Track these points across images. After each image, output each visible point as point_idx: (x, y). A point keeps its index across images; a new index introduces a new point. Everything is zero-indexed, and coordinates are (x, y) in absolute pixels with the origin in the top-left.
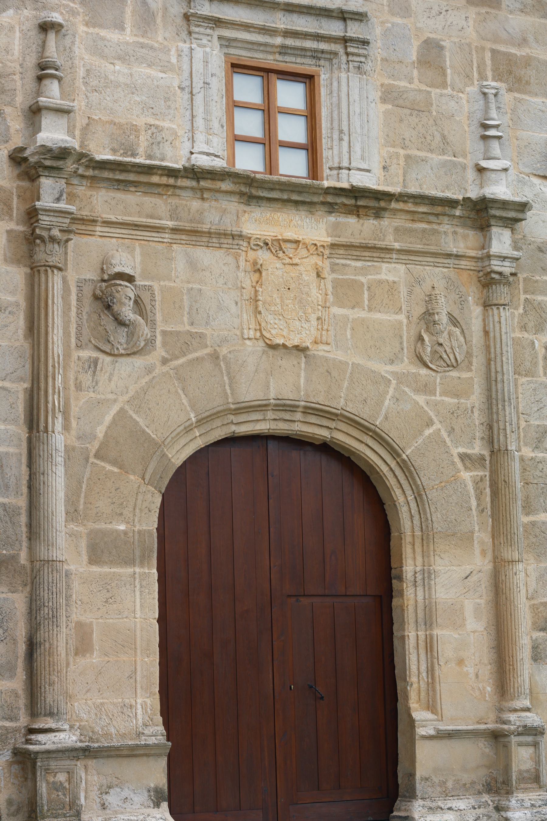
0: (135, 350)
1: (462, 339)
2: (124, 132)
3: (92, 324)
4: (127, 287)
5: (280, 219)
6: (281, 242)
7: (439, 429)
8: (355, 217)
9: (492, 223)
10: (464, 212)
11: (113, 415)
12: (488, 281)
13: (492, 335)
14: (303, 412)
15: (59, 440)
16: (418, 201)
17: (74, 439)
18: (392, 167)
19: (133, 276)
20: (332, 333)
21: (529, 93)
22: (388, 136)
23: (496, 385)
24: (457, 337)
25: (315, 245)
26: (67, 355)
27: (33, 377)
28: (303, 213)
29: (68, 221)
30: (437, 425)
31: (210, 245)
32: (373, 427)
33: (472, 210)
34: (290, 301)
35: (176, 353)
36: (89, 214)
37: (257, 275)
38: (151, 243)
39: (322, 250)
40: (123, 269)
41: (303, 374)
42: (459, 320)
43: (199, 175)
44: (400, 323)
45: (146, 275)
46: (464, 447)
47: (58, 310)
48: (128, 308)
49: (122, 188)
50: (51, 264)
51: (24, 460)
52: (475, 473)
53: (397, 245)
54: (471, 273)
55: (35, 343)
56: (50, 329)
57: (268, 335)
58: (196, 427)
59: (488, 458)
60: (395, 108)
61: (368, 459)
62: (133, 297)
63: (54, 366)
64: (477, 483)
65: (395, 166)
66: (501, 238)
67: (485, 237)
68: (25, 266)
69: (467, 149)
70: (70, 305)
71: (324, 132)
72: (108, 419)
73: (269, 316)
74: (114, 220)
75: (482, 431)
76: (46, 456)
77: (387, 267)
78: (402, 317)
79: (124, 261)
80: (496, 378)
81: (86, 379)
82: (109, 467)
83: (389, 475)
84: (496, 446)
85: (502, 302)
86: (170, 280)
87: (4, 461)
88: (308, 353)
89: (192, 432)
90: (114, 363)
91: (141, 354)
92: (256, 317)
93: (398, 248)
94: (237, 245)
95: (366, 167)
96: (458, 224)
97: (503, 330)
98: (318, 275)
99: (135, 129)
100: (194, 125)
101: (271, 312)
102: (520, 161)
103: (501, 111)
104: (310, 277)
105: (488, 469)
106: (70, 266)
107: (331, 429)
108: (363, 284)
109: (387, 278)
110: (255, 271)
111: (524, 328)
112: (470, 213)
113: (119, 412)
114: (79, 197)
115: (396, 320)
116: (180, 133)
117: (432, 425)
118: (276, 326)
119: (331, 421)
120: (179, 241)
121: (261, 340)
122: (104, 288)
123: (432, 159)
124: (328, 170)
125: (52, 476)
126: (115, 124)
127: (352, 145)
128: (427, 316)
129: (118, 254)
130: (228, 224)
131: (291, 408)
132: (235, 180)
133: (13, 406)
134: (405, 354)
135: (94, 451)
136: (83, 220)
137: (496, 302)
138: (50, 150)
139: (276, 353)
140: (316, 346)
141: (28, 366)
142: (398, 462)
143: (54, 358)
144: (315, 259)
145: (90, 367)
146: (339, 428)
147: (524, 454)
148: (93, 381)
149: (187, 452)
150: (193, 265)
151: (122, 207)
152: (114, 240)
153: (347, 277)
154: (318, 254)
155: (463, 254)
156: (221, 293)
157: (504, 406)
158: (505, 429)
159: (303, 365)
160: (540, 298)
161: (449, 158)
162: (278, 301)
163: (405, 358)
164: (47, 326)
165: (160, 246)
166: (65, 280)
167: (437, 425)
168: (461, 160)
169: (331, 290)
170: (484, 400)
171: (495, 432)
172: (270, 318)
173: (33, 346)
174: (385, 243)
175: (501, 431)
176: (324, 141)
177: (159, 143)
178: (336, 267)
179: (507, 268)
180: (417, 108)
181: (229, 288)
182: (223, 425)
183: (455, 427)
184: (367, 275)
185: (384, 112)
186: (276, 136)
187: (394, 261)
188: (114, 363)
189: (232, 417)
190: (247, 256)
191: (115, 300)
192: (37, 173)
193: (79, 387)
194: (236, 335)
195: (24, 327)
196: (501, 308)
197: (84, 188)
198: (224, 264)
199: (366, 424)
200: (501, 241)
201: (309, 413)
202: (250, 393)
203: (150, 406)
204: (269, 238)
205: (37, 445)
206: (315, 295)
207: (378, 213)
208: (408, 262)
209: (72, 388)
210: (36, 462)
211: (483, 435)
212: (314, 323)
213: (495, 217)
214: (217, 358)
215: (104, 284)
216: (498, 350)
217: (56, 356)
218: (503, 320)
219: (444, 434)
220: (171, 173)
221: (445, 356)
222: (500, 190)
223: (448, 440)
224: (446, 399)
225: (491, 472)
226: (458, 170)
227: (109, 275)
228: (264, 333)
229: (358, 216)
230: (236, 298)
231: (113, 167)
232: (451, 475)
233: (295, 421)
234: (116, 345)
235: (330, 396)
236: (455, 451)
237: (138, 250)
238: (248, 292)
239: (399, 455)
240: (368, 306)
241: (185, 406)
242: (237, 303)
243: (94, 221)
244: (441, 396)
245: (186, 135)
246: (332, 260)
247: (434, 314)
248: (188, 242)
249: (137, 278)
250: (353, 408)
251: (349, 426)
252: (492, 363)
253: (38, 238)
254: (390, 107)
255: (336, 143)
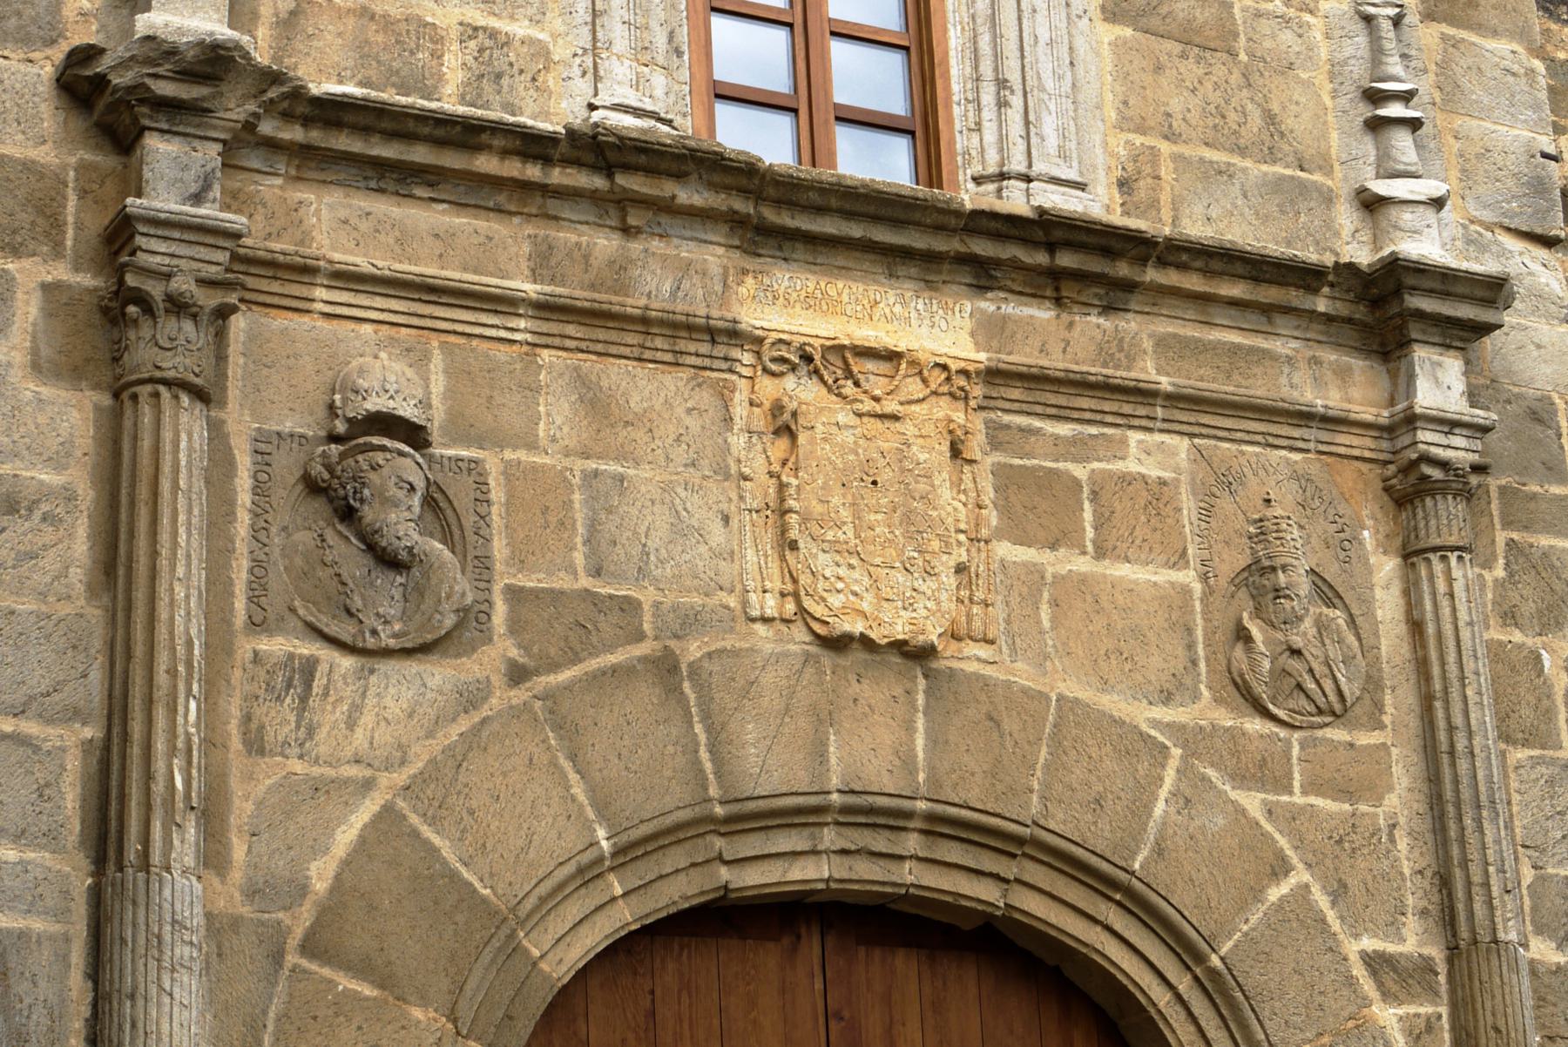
0: (429, 637)
1: (1351, 639)
2: (398, 42)
3: (298, 561)
4: (401, 454)
5: (845, 298)
6: (848, 355)
7: (1307, 886)
8: (1048, 304)
9: (1414, 335)
10: (1338, 304)
11: (359, 825)
12: (1411, 486)
13: (1431, 629)
14: (923, 832)
15: (183, 892)
16: (1216, 265)
17: (237, 894)
18: (1141, 183)
19: (422, 428)
20: (998, 612)
21: (1478, 28)
22: (1125, 103)
23: (1453, 764)
24: (1339, 632)
25: (945, 367)
26: (219, 644)
27: (110, 705)
28: (908, 285)
29: (222, 257)
30: (1300, 875)
31: (648, 355)
32: (1123, 876)
33: (1359, 299)
34: (880, 517)
35: (552, 651)
36: (291, 248)
37: (783, 443)
38: (475, 342)
39: (962, 382)
40: (391, 404)
41: (920, 723)
42: (1340, 590)
43: (612, 156)
44: (1185, 591)
45: (461, 431)
46: (1376, 936)
47: (190, 511)
48: (407, 515)
49: (391, 187)
50: (171, 374)
51: (78, 956)
52: (1412, 1009)
53: (1165, 383)
54: (1365, 467)
55: (120, 606)
56: (163, 563)
57: (818, 610)
58: (612, 869)
59: (1442, 968)
60: (1138, 35)
61: (1112, 970)
62: (420, 484)
63: (172, 672)
64: (1418, 1037)
65: (1149, 180)
66: (1439, 374)
67: (1393, 376)
68: (96, 387)
69: (1333, 152)
70: (231, 503)
71: (955, 87)
72: (345, 837)
73: (821, 556)
74: (366, 268)
75: (1420, 893)
76: (142, 941)
77: (1140, 442)
78: (1188, 577)
79: (392, 378)
80: (1452, 745)
81: (280, 719)
82: (345, 983)
83: (1175, 1016)
84: (1464, 933)
85: (1453, 540)
86: (532, 446)
87: (13, 960)
88: (934, 665)
89: (600, 883)
90: (362, 674)
91: (445, 654)
92: (783, 558)
93: (1170, 389)
94: (726, 359)
95: (1072, 175)
96: (1321, 338)
97: (1463, 616)
98: (956, 452)
99: (433, 36)
100: (600, 35)
101: (826, 546)
102: (1467, 192)
103: (1413, 64)
104: (931, 454)
105: (1445, 997)
106: (233, 392)
107: (1006, 881)
108: (1077, 483)
109: (1143, 470)
110: (777, 432)
111: (1510, 617)
112: (1353, 307)
113: (378, 819)
114: (264, 205)
115: (1172, 583)
116: (559, 52)
117: (1287, 873)
118: (840, 585)
119: (1004, 859)
120: (557, 342)
121: (800, 623)
122: (335, 459)
123: (1244, 170)
124: (971, 185)
125: (159, 1005)
126: (372, 18)
127: (1032, 118)
128: (1256, 578)
129: (378, 364)
130: (697, 303)
131: (891, 819)
132: (716, 178)
133: (47, 792)
134: (1203, 677)
135: (299, 933)
136: (272, 264)
137: (1438, 542)
138: (172, 52)
139: (845, 661)
140: (954, 645)
141: (96, 676)
142: (1196, 978)
143: (173, 649)
144: (943, 409)
145: (289, 685)
146: (1027, 878)
147: (1537, 957)
148: (298, 727)
149: (589, 942)
150: (596, 405)
151: (391, 241)
152: (367, 328)
153: (1035, 462)
154: (951, 394)
155: (1343, 414)
156: (680, 490)
157: (1479, 821)
158: (1486, 885)
159: (921, 699)
160: (1545, 541)
161: (1289, 172)
162: (845, 514)
163: (1202, 687)
164: (154, 554)
165: (502, 353)
166: (216, 430)
167: (1300, 875)
168: (1316, 177)
169: (992, 495)
170: (1422, 807)
171: (1460, 894)
172: (823, 562)
173: (114, 615)
174: (1133, 375)
175: (1475, 889)
176: (957, 111)
177: (499, 76)
178: (1002, 436)
179: (1459, 450)
180: (1197, 40)
181: (705, 477)
182: (693, 865)
183: (1349, 881)
184: (1087, 460)
185: (1115, 44)
186: (828, 92)
187: (1159, 425)
188: (362, 674)
189: (719, 843)
190: (753, 392)
191: (366, 492)
192: (136, 120)
193: (256, 745)
194: (727, 607)
195: (87, 562)
196: (1453, 558)
197: (279, 181)
198: (689, 411)
199: (1105, 867)
200: (1439, 383)
201: (942, 835)
202: (768, 765)
203: (474, 804)
204: (817, 343)
205: (117, 907)
206: (950, 505)
207: (1116, 296)
208: (1196, 430)
209: (236, 743)
210: (111, 960)
211: (1424, 903)
212: (950, 580)
213: (1420, 315)
214: (674, 669)
215: (335, 449)
216: (1452, 668)
217: (180, 642)
218: (1459, 587)
219: (1321, 900)
220: (533, 145)
221: (1311, 685)
222: (1426, 244)
223: (1331, 915)
224: (1319, 802)
225: (1454, 1006)
226: (1313, 204)
227: (349, 420)
228: (808, 603)
229: (1058, 301)
230: (724, 506)
231: (361, 119)
232: (1345, 1014)
233: (901, 858)
234: (370, 621)
235: (1000, 787)
236: (1353, 948)
237: (437, 361)
238: (760, 490)
239: (1200, 958)
240: (1094, 542)
241: (581, 806)
242: (726, 519)
243: (305, 271)
244: (1305, 793)
245: (578, 60)
246: (992, 415)
247: (1274, 569)
248: (583, 345)
249: (435, 436)
250: (1065, 822)
251: (1055, 874)
252: (1438, 704)
253: (135, 303)
254: (1128, 32)
255: (989, 114)
